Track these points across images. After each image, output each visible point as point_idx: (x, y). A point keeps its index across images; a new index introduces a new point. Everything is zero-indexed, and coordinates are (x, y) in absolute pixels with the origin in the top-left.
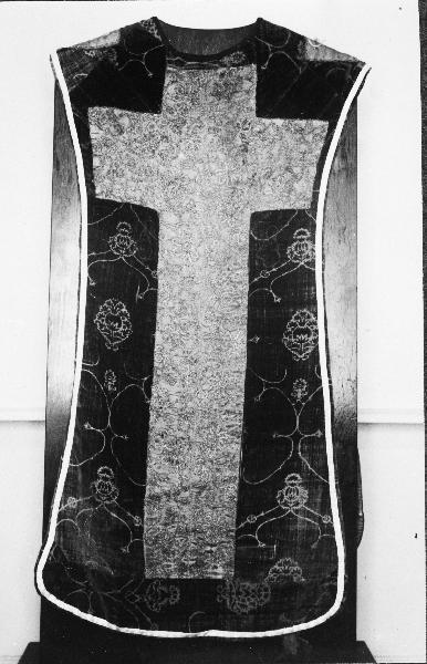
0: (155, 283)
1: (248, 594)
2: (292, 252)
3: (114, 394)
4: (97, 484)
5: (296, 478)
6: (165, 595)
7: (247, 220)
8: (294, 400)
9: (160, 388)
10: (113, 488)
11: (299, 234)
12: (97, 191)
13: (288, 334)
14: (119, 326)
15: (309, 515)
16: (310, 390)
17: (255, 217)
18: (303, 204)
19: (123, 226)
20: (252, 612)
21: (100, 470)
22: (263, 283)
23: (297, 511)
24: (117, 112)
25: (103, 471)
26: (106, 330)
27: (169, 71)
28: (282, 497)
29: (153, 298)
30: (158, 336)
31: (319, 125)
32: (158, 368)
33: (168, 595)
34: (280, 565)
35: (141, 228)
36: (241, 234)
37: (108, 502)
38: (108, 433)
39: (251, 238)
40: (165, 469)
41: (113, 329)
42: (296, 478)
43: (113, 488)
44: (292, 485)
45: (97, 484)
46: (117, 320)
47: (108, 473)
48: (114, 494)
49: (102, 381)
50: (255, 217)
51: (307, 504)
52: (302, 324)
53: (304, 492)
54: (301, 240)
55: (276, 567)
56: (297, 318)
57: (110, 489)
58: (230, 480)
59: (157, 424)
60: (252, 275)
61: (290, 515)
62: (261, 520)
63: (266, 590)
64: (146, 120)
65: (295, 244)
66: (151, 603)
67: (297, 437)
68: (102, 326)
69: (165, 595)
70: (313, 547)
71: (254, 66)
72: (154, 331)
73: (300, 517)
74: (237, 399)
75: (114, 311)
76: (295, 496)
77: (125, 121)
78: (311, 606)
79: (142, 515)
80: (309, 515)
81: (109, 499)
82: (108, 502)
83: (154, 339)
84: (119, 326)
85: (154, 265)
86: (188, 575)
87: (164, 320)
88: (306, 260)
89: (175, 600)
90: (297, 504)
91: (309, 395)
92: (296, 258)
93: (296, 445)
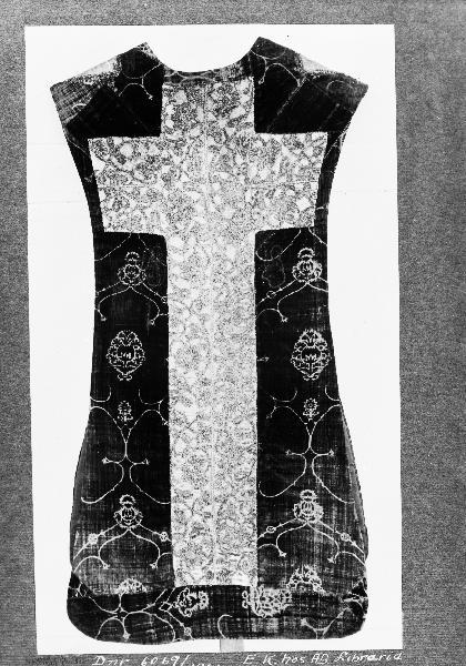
0: (165, 309)
1: (271, 599)
2: (297, 272)
3: (130, 424)
4: (120, 512)
5: (308, 253)
6: (195, 601)
7: (252, 239)
8: (305, 419)
9: (176, 408)
10: (136, 513)
11: (303, 253)
12: (106, 222)
13: (296, 354)
14: (132, 356)
15: (325, 530)
16: (322, 409)
17: (260, 236)
18: (301, 214)
19: (130, 256)
20: (276, 616)
21: (121, 499)
22: (271, 303)
23: (313, 283)
24: (117, 140)
25: (124, 500)
26: (119, 363)
27: (166, 90)
28: (298, 511)
29: (163, 324)
30: (171, 361)
31: (320, 137)
32: (176, 250)
33: (198, 600)
34: (304, 338)
35: (148, 254)
36: (244, 252)
37: (133, 527)
38: (126, 464)
39: (256, 259)
40: (188, 486)
41: (125, 359)
42: (308, 253)
43: (136, 513)
44: (307, 500)
45: (120, 512)
46: (130, 350)
47: (130, 500)
48: (138, 517)
49: (116, 414)
50: (260, 236)
51: (324, 520)
52: (312, 344)
53: (319, 509)
54: (307, 259)
55: (301, 341)
56: (304, 338)
57: (137, 272)
58: (250, 493)
59: (177, 445)
60: (259, 296)
61: (307, 527)
62: (279, 530)
63: (287, 595)
64: (147, 147)
65: (300, 263)
66: (183, 609)
67: (310, 456)
68: (113, 359)
69: (195, 601)
70: (331, 560)
71: (251, 78)
72: (167, 356)
73: (317, 531)
74: (249, 425)
75: (126, 342)
76: (310, 511)
77: (127, 150)
78: (333, 619)
79: (169, 531)
80: (325, 530)
81: (135, 523)
82: (133, 527)
83: (167, 363)
84: (132, 356)
85: (163, 290)
86: (214, 582)
87: (176, 345)
88: (312, 280)
89: (204, 603)
90: (313, 519)
91: (320, 415)
92: (301, 278)
93: (309, 462)
